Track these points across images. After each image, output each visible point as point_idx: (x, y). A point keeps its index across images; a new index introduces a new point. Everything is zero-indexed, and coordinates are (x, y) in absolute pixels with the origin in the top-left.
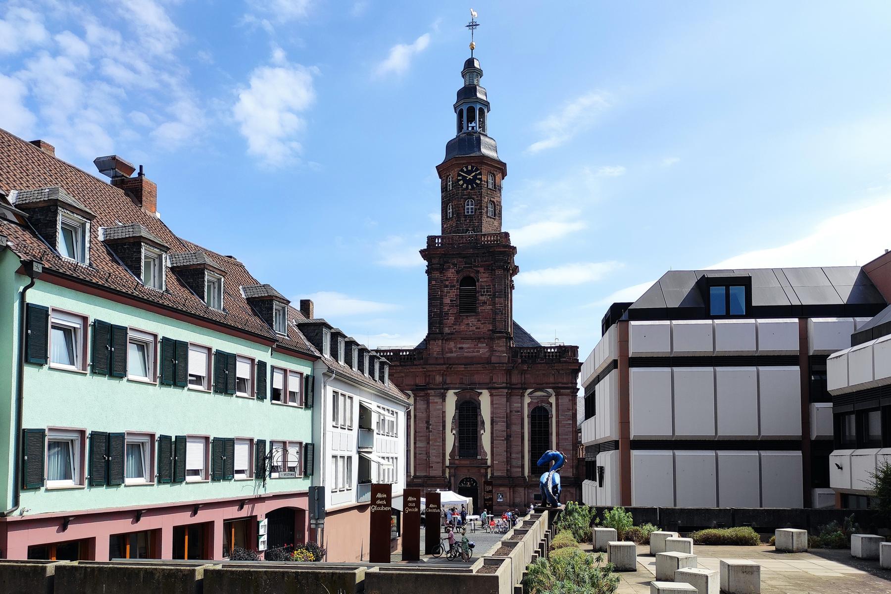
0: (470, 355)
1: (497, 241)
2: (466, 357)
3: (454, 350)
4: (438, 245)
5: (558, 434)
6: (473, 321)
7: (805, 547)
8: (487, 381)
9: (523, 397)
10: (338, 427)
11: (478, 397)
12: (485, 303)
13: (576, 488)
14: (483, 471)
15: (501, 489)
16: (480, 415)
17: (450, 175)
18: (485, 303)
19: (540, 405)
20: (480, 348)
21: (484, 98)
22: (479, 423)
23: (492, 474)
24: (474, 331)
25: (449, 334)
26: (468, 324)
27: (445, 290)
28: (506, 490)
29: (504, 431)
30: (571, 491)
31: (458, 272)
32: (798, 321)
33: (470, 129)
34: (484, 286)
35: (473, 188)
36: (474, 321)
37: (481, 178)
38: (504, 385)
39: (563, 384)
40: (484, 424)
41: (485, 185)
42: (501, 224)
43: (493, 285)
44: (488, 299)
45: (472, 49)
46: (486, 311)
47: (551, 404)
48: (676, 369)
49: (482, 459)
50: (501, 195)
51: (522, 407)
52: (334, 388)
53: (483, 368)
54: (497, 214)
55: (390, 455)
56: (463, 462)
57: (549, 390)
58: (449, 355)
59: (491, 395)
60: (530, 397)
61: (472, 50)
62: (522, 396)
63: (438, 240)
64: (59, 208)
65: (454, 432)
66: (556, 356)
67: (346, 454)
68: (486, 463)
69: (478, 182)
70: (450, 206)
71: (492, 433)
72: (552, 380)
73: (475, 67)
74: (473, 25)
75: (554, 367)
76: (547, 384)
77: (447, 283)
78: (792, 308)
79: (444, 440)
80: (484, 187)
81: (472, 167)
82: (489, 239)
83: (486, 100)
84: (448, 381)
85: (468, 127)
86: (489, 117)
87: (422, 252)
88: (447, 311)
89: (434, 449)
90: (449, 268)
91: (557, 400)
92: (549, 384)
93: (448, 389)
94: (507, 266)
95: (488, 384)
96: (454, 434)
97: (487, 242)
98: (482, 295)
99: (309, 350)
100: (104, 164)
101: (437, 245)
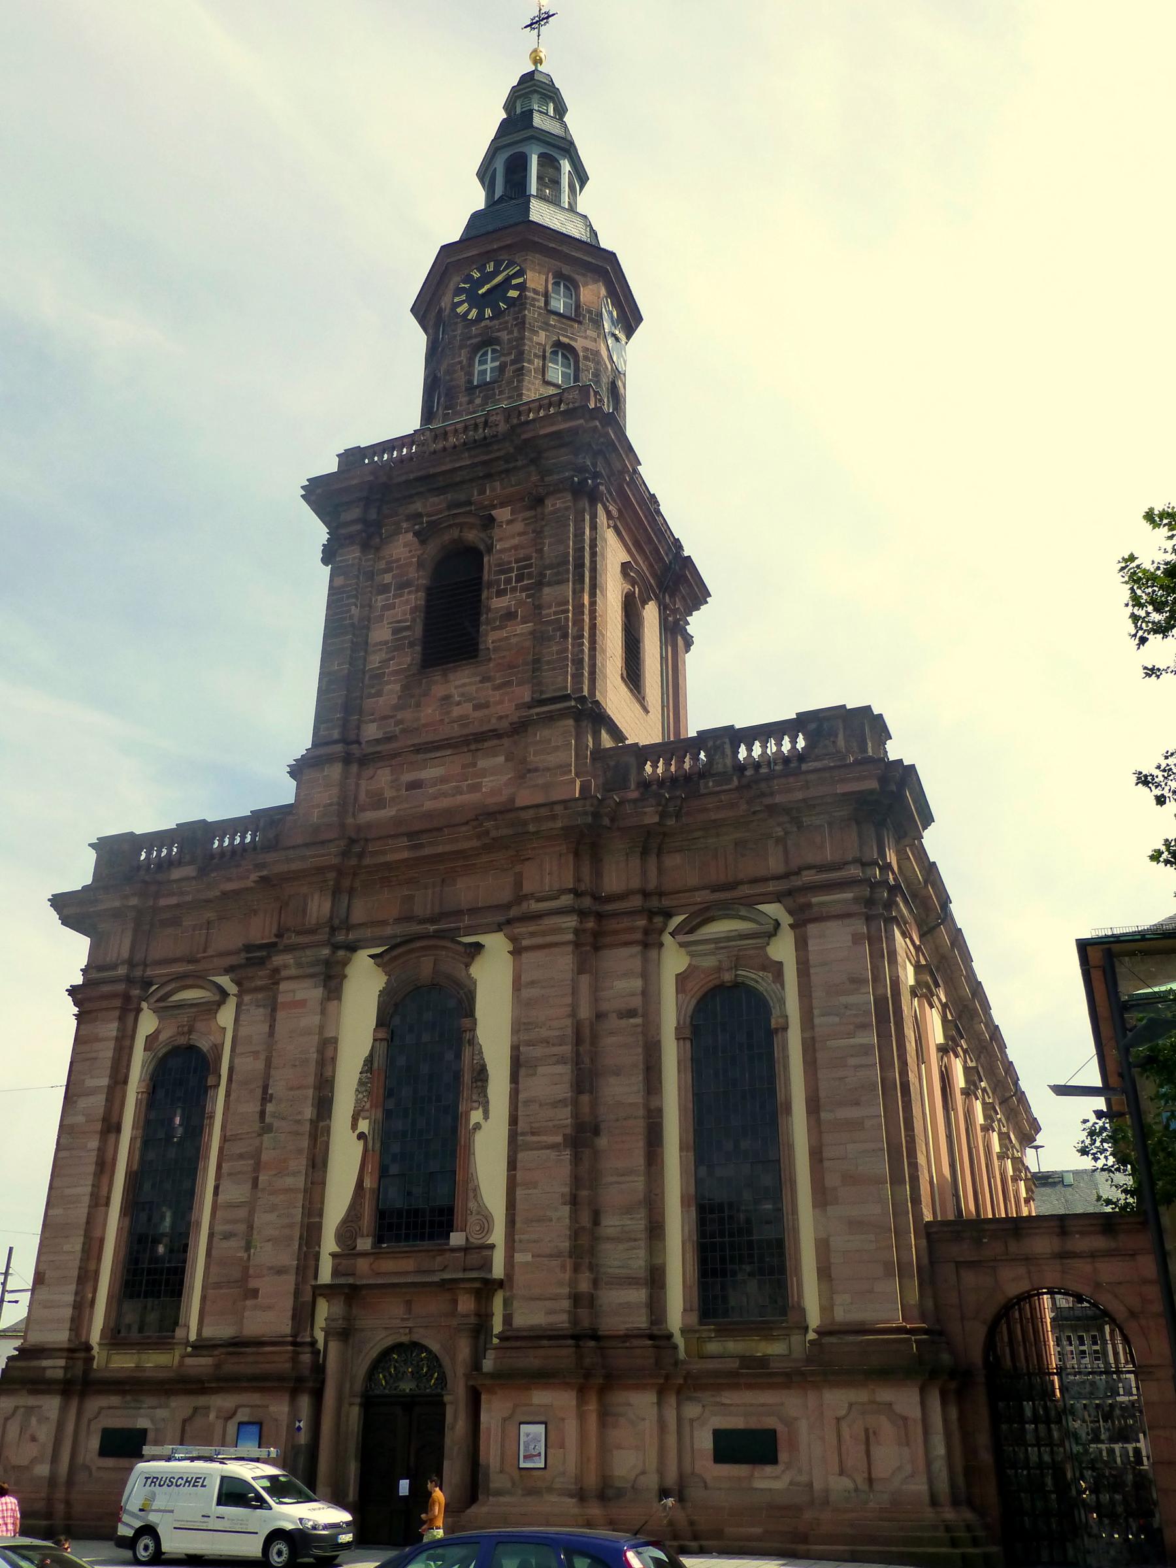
0: (445, 803)
2: (429, 815)
3: (389, 794)
5: (814, 1106)
6: (464, 685)
7: (563, 1195)
8: (506, 896)
9: (653, 954)
11: (468, 965)
12: (510, 615)
13: (923, 1391)
14: (466, 1304)
15: (541, 1397)
16: (473, 1041)
18: (510, 615)
19: (727, 977)
20: (484, 773)
22: (467, 1078)
23: (508, 1319)
24: (467, 717)
25: (378, 741)
26: (447, 698)
27: (380, 601)
28: (561, 1400)
29: (562, 1102)
30: (898, 1408)
31: (422, 537)
34: (510, 563)
35: (498, 314)
36: (470, 684)
38: (566, 900)
39: (821, 868)
40: (486, 1080)
43: (537, 551)
44: (521, 603)
46: (514, 640)
49: (466, 1249)
51: (650, 993)
53: (479, 837)
56: (388, 1265)
57: (773, 910)
58: (369, 816)
65: (364, 1126)
68: (487, 1265)
71: (513, 1120)
72: (774, 863)
74: (540, 21)
75: (772, 794)
76: (755, 881)
77: (388, 578)
79: (318, 1163)
84: (359, 914)
88: (378, 668)
89: (273, 1208)
90: (397, 532)
91: (801, 945)
92: (765, 880)
93: (353, 948)
95: (508, 906)
96: (361, 1136)
98: (500, 593)
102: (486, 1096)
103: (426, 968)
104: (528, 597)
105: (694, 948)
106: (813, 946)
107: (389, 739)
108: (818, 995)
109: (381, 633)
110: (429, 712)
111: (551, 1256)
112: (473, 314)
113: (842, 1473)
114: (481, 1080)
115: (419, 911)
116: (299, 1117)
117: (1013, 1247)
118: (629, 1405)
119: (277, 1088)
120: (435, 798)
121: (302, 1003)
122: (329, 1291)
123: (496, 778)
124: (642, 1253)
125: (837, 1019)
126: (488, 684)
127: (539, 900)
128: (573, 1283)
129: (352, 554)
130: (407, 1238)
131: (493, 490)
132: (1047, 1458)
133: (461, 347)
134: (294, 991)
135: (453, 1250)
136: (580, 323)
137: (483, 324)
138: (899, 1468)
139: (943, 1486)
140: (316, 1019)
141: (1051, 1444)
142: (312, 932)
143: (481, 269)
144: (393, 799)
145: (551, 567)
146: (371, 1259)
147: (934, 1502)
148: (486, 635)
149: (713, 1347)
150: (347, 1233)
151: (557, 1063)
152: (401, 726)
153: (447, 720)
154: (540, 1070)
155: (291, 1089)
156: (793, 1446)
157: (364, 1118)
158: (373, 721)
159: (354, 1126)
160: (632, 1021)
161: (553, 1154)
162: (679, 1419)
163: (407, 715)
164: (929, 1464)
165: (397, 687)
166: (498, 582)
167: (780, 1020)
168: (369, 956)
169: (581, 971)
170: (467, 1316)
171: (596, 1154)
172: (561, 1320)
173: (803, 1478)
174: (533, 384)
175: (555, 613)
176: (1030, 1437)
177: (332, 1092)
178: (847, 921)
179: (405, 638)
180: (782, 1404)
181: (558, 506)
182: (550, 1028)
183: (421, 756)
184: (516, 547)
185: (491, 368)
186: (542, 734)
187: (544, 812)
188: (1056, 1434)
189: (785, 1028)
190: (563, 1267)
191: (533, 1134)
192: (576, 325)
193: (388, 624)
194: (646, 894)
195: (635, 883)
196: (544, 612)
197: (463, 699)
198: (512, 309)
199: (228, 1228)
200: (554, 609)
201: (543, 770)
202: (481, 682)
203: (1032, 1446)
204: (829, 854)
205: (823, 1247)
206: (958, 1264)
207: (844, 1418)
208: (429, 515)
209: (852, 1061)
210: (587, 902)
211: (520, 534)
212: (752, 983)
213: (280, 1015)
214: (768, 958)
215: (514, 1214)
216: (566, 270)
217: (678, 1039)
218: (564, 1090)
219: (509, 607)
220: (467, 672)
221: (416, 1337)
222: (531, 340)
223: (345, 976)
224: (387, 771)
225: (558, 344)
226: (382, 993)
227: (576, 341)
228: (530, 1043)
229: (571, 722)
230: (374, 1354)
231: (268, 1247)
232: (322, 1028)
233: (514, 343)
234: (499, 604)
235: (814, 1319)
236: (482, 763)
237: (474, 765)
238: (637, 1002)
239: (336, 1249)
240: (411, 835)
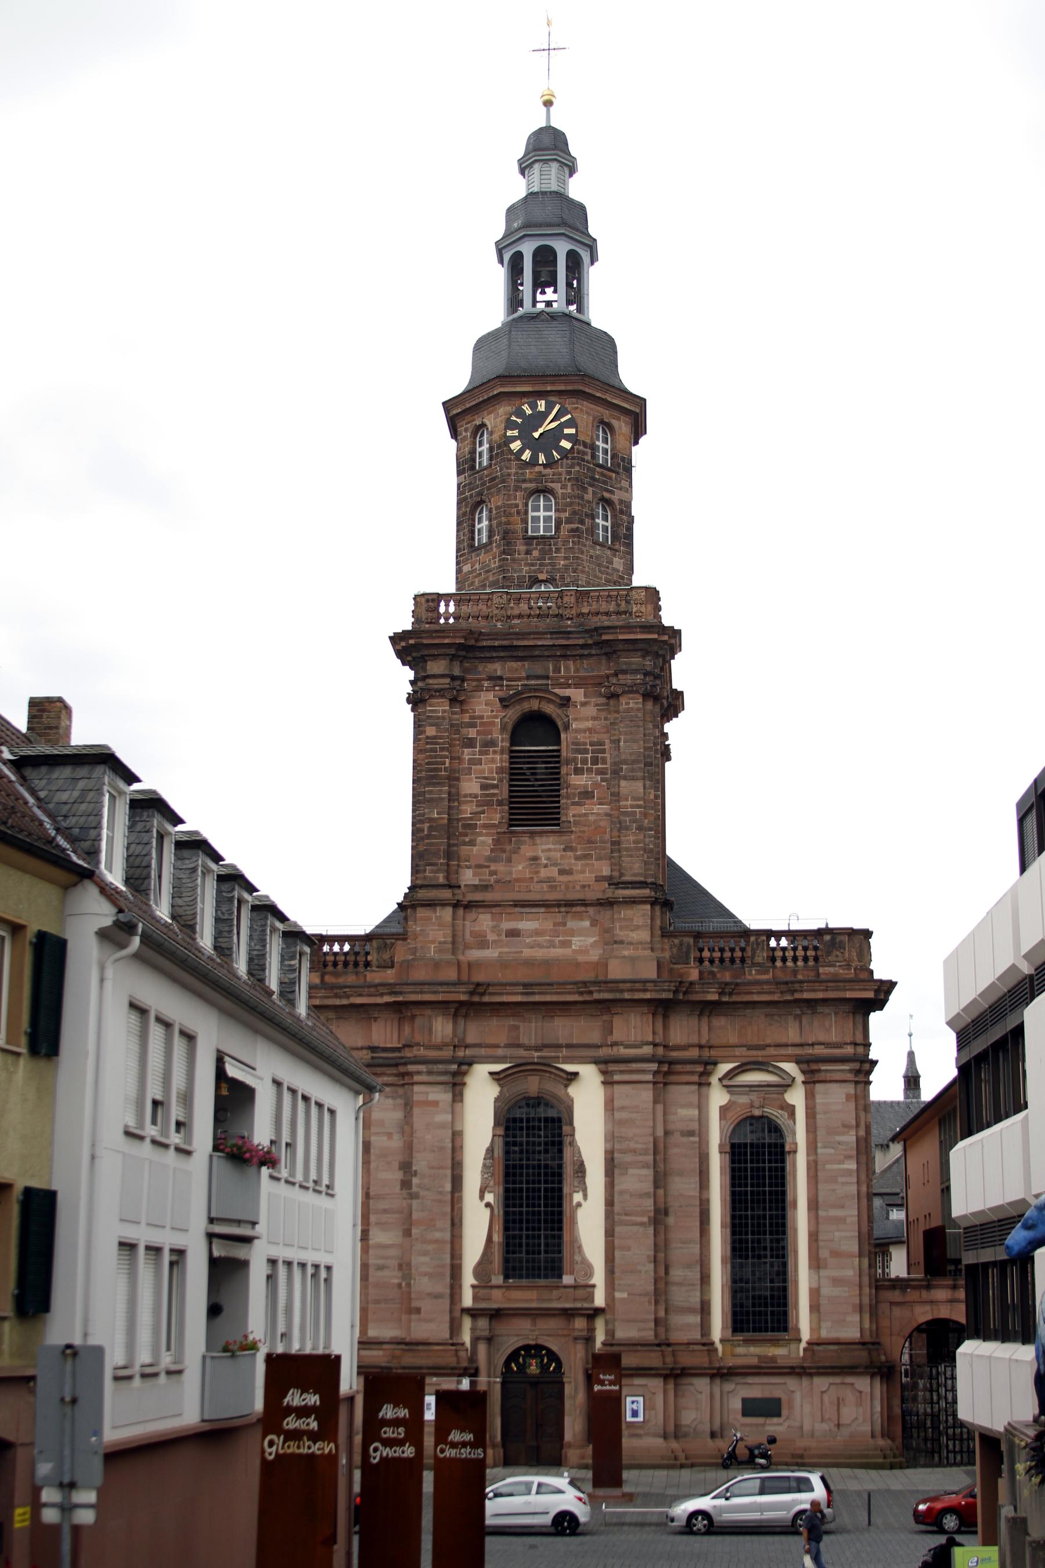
3: (491, 937)
5: (814, 1205)
6: (549, 850)
7: (648, 1256)
9: (704, 1089)
12: (587, 795)
16: (573, 1143)
18: (587, 795)
19: (757, 1113)
20: (572, 933)
25: (475, 888)
26: (535, 859)
27: (467, 754)
28: (655, 1384)
29: (647, 1194)
34: (585, 744)
36: (555, 850)
38: (647, 1050)
43: (612, 742)
46: (591, 818)
47: (791, 1110)
50: (631, 486)
51: (703, 1120)
57: (785, 1066)
63: (447, 605)
65: (489, 1197)
67: (167, 1239)
68: (591, 1298)
71: (609, 1203)
77: (472, 733)
79: (456, 1223)
88: (471, 819)
89: (425, 1253)
90: (479, 689)
91: (810, 1096)
92: (786, 1045)
96: (488, 1205)
98: (578, 771)
102: (585, 1183)
103: (532, 1085)
104: (602, 780)
105: (732, 1089)
106: (819, 1099)
107: (485, 888)
108: (821, 1134)
110: (519, 868)
111: (640, 1295)
112: (526, 455)
113: (822, 1421)
114: (581, 1172)
115: (524, 1040)
116: (440, 1189)
117: (925, 1294)
118: (692, 1384)
119: (420, 1163)
120: (532, 947)
121: (435, 1103)
122: (473, 1313)
123: (583, 938)
124: (698, 1294)
125: (833, 1151)
126: (570, 854)
127: (627, 1047)
128: (656, 1312)
129: (440, 707)
130: (527, 1277)
131: (567, 668)
132: (929, 1410)
133: (517, 488)
134: (427, 1093)
135: (565, 1287)
136: (617, 473)
137: (537, 469)
138: (856, 1419)
139: (878, 1428)
140: (448, 1117)
141: (932, 1403)
142: (438, 1047)
143: (534, 406)
144: (494, 941)
145: (625, 762)
146: (504, 1290)
147: (873, 1436)
148: (567, 809)
149: (741, 1350)
150: (480, 1270)
151: (643, 1167)
152: (495, 877)
153: (536, 879)
154: (631, 1171)
155: (432, 1168)
156: (791, 1407)
157: (489, 1192)
158: (468, 867)
159: (482, 1197)
160: (692, 1139)
161: (641, 1229)
162: (721, 1392)
163: (500, 867)
164: (872, 1415)
165: (489, 840)
166: (575, 760)
167: (792, 1146)
168: (491, 1073)
169: (655, 1102)
170: (581, 1330)
171: (666, 1228)
172: (649, 1335)
173: (797, 1424)
174: (585, 546)
175: (632, 806)
176: (920, 1399)
177: (462, 1171)
178: (843, 1085)
179: (494, 795)
180: (785, 1384)
181: (631, 705)
182: (637, 1142)
183: (517, 909)
184: (590, 730)
185: (544, 517)
186: (625, 913)
187: (638, 986)
188: (935, 1398)
189: (795, 1152)
190: (650, 1302)
191: (626, 1214)
193: (476, 778)
194: (701, 1047)
195: (694, 1040)
196: (621, 803)
197: (549, 863)
198: (565, 461)
199: (380, 1262)
200: (629, 802)
201: (628, 944)
202: (564, 850)
203: (921, 1403)
204: (834, 1037)
205: (815, 1293)
206: (892, 1304)
207: (825, 1392)
208: (509, 680)
209: (841, 1180)
210: (660, 1051)
211: (594, 719)
212: (774, 1118)
213: (416, 1111)
214: (785, 1101)
215: (614, 1266)
216: (606, 414)
217: (721, 1152)
218: (648, 1186)
219: (586, 786)
220: (551, 839)
221: (540, 1342)
224: (489, 916)
225: (603, 499)
226: (497, 1100)
227: (612, 492)
228: (623, 1152)
229: (648, 907)
230: (509, 1351)
231: (425, 1280)
232: (453, 1122)
233: (568, 500)
234: (580, 781)
235: (805, 1335)
236: (572, 924)
237: (565, 924)
238: (695, 1126)
239: (475, 1282)
240: (525, 985)
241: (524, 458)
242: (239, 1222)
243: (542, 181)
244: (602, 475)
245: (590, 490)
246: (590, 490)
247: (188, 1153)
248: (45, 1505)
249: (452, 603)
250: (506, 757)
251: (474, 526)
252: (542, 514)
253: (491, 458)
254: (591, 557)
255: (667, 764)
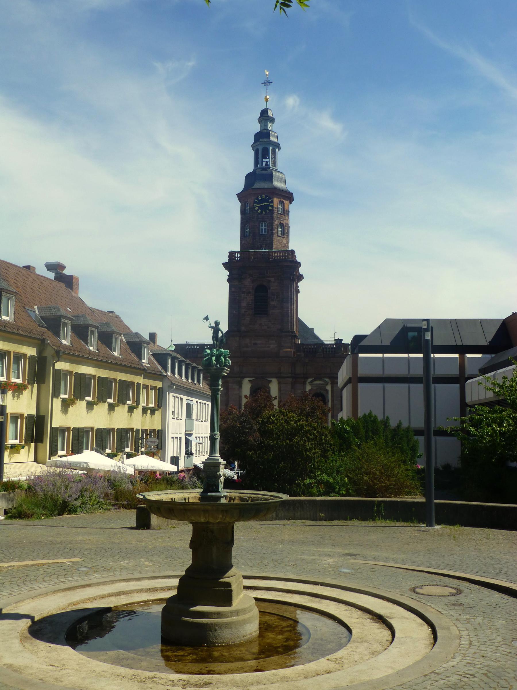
1: (285, 257)
4: (238, 259)
10: (174, 419)
17: (247, 201)
21: (276, 140)
32: (458, 356)
33: (264, 163)
37: (273, 205)
38: (289, 375)
41: (275, 210)
42: (288, 241)
45: (267, 100)
47: (327, 391)
48: (386, 385)
50: (289, 218)
52: (173, 394)
54: (286, 233)
55: (200, 435)
57: (326, 379)
59: (279, 383)
60: (311, 385)
61: (267, 102)
62: (304, 384)
63: (238, 255)
64: (62, 319)
66: (332, 351)
67: (178, 436)
69: (270, 208)
70: (247, 226)
73: (269, 116)
77: (244, 290)
78: (457, 346)
80: (275, 212)
81: (266, 197)
82: (279, 255)
83: (277, 142)
85: (263, 161)
86: (280, 154)
87: (224, 264)
91: (332, 388)
94: (293, 278)
97: (277, 258)
98: (273, 300)
99: (161, 372)
100: (50, 267)
101: (236, 259)
109: (244, 304)
136: (284, 215)
137: (262, 215)
189: (328, 402)
192: (284, 216)
222: (275, 224)
223: (242, 383)
226: (250, 387)
227: (283, 221)
241: (259, 212)
242: (191, 431)
243: (204, 438)
244: (280, 216)
245: (277, 221)
246: (277, 221)
247: (182, 420)
248: (178, 469)
249: (239, 254)
250: (253, 296)
251: (245, 230)
252: (264, 228)
253: (250, 211)
254: (277, 240)
255: (299, 294)
